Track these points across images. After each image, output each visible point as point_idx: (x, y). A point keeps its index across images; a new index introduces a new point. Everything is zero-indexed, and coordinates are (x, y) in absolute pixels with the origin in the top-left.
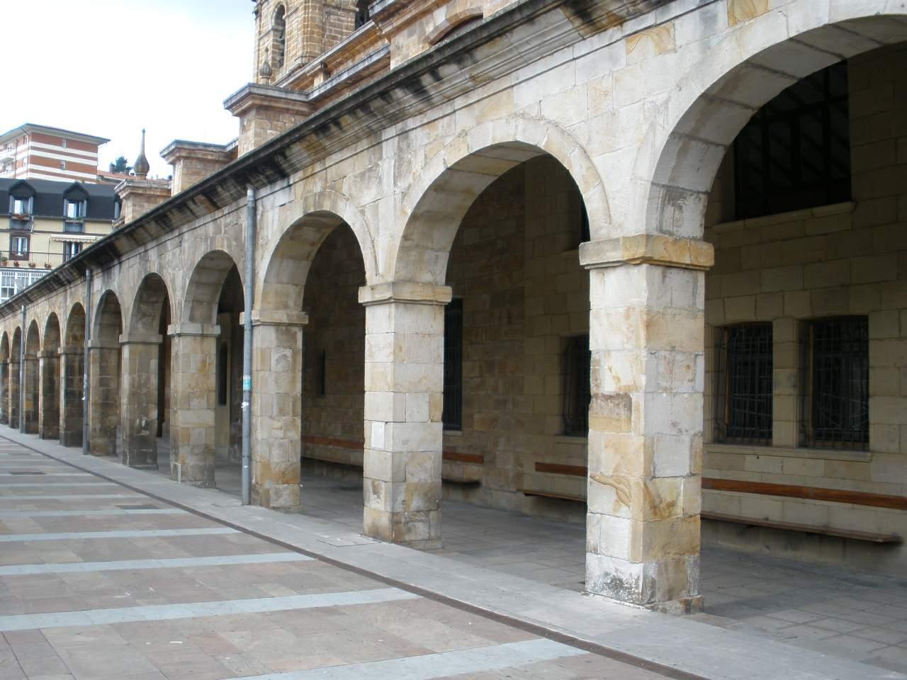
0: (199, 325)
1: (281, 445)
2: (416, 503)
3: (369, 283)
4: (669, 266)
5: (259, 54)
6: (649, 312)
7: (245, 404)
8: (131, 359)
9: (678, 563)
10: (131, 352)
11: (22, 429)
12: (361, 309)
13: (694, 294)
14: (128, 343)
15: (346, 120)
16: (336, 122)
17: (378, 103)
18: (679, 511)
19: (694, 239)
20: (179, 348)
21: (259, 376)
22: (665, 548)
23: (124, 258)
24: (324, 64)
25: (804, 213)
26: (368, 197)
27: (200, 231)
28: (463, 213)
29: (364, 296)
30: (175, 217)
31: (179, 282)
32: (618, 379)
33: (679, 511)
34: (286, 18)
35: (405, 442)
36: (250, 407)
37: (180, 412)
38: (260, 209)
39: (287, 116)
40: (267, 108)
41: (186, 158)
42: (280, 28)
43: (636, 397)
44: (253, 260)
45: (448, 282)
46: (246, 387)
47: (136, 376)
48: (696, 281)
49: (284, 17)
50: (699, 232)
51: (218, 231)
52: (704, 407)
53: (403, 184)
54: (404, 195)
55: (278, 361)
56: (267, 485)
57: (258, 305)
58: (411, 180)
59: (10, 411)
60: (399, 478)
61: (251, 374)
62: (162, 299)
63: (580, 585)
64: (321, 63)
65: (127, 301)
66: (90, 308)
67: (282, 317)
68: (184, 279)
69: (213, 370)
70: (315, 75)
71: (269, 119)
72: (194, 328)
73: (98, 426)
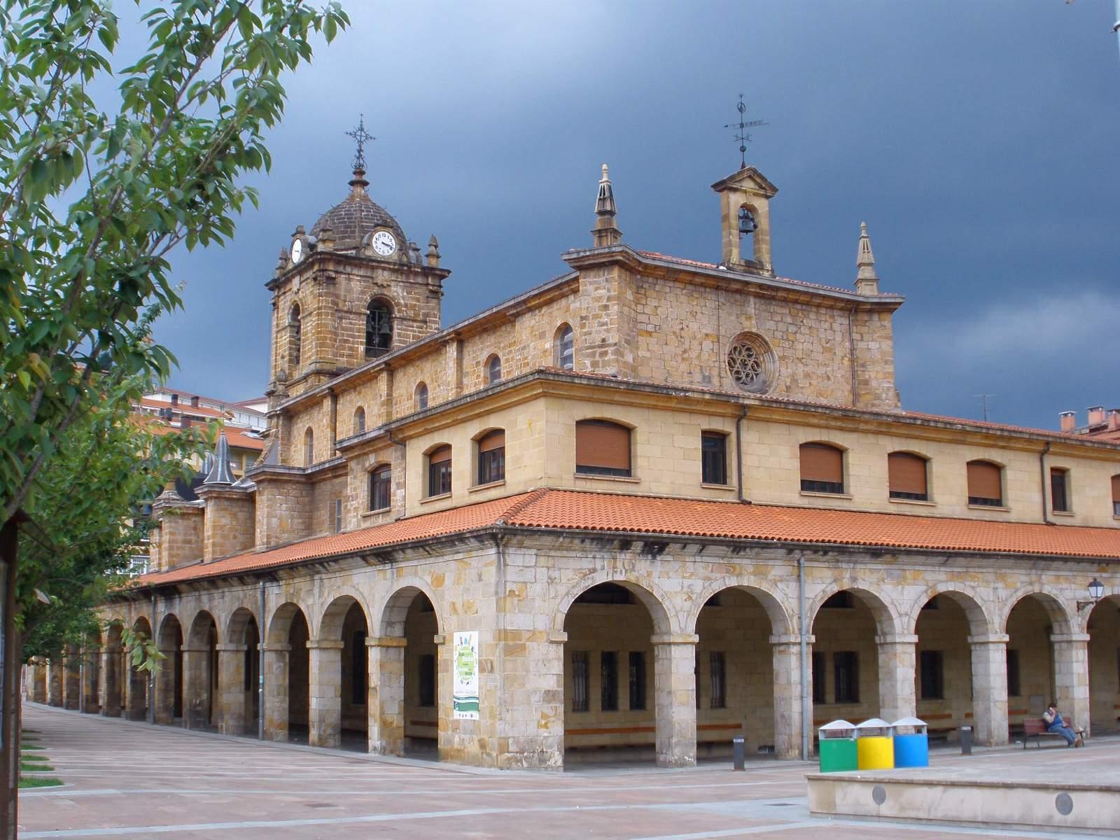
0: (235, 645)
1: (278, 710)
2: (329, 731)
4: (388, 647)
6: (381, 661)
7: (260, 690)
8: (190, 662)
9: (395, 742)
10: (190, 657)
11: (83, 709)
12: (308, 650)
13: (400, 655)
14: (188, 651)
15: (300, 568)
16: (296, 567)
17: (310, 566)
18: (395, 725)
19: (400, 637)
20: (223, 657)
21: (267, 676)
22: (389, 736)
23: (183, 595)
24: (331, 389)
26: (310, 602)
27: (236, 594)
28: (346, 612)
29: (308, 645)
30: (220, 583)
31: (223, 619)
33: (395, 725)
35: (324, 706)
36: (263, 692)
37: (224, 695)
38: (266, 593)
39: (290, 485)
40: (275, 481)
41: (216, 498)
42: (297, 324)
43: (378, 688)
44: (264, 618)
45: (342, 640)
46: (261, 681)
47: (193, 672)
48: (400, 651)
50: (402, 635)
51: (245, 597)
52: (916, 679)
53: (321, 600)
54: (322, 604)
55: (277, 669)
56: (272, 730)
57: (266, 641)
59: (65, 694)
60: (322, 720)
61: (263, 675)
62: (209, 623)
63: (365, 750)
64: (329, 388)
65: (187, 624)
66: (155, 623)
67: (278, 647)
68: (226, 617)
69: (243, 670)
70: (324, 397)
71: (277, 488)
72: (232, 647)
73: (161, 705)
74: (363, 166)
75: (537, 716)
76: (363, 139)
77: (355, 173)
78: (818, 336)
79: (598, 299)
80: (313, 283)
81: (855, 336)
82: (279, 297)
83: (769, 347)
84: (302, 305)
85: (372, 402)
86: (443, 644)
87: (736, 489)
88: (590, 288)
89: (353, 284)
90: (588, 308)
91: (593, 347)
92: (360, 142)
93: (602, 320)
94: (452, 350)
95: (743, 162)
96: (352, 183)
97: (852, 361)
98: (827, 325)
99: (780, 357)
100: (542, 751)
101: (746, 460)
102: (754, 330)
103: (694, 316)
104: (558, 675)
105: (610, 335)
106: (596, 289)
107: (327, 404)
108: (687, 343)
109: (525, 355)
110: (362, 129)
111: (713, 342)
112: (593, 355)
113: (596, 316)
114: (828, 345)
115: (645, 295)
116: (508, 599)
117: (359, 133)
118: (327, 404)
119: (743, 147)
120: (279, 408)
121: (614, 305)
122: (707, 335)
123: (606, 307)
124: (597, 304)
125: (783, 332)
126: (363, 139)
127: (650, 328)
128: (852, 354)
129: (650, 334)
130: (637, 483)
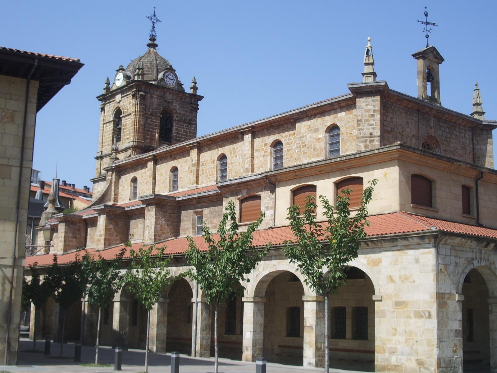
3: (245, 296)
5: (103, 132)
25: (354, 280)
32: (310, 323)
34: (122, 117)
49: (121, 116)
58: (259, 272)
64: (153, 155)
74: (155, 36)
75: (452, 345)
76: (155, 21)
77: (150, 40)
78: (459, 140)
79: (368, 111)
80: (132, 97)
81: (475, 142)
82: (105, 104)
83: (439, 144)
84: (123, 110)
85: (184, 164)
86: (381, 301)
87: (476, 218)
88: (363, 105)
89: (154, 100)
90: (361, 115)
91: (366, 137)
92: (153, 22)
93: (370, 122)
94: (248, 138)
95: (427, 44)
96: (149, 45)
97: (473, 155)
98: (462, 135)
99: (443, 150)
100: (455, 367)
101: (481, 203)
102: (433, 135)
103: (408, 125)
104: (460, 320)
105: (375, 131)
106: (367, 105)
107: (150, 164)
108: (405, 139)
109: (303, 141)
110: (154, 16)
111: (416, 139)
112: (366, 141)
113: (367, 120)
114: (464, 146)
115: (387, 111)
116: (440, 274)
117: (153, 17)
118: (150, 164)
119: (427, 35)
120: (114, 165)
121: (377, 115)
122: (413, 135)
123: (373, 116)
124: (367, 114)
125: (445, 137)
126: (155, 21)
127: (389, 129)
128: (473, 151)
129: (389, 132)
130: (437, 212)
